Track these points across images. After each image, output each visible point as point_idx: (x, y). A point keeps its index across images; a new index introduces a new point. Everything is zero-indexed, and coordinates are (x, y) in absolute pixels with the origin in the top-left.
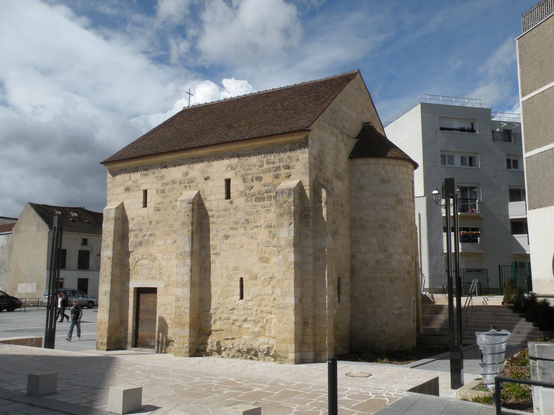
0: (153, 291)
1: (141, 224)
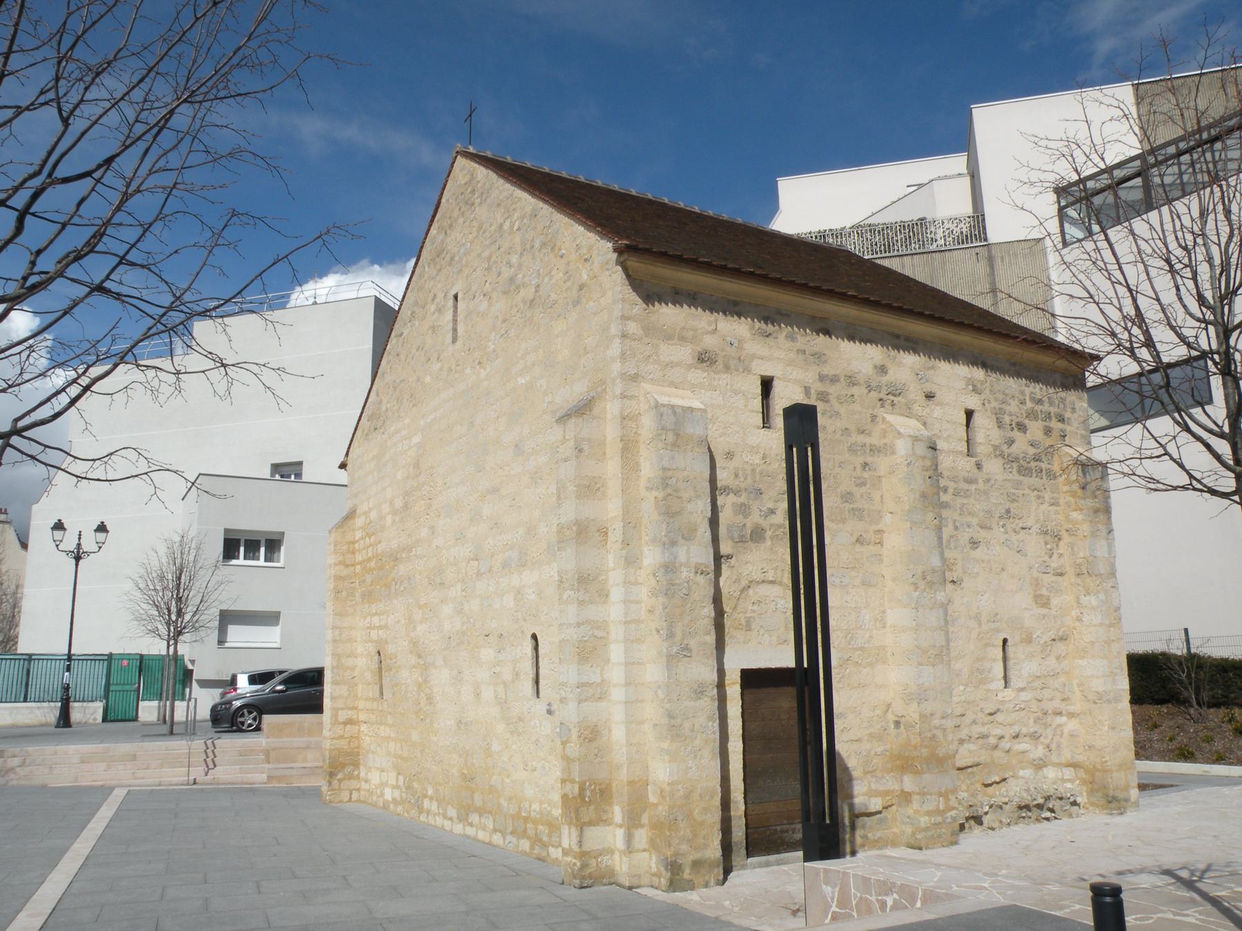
1: (758, 477)
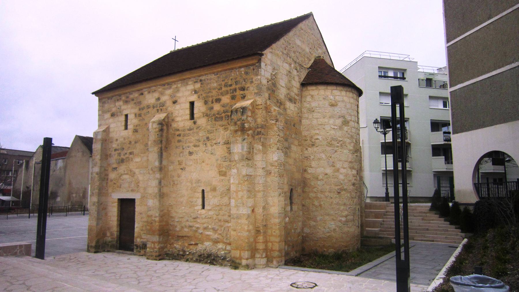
0: (133, 201)
